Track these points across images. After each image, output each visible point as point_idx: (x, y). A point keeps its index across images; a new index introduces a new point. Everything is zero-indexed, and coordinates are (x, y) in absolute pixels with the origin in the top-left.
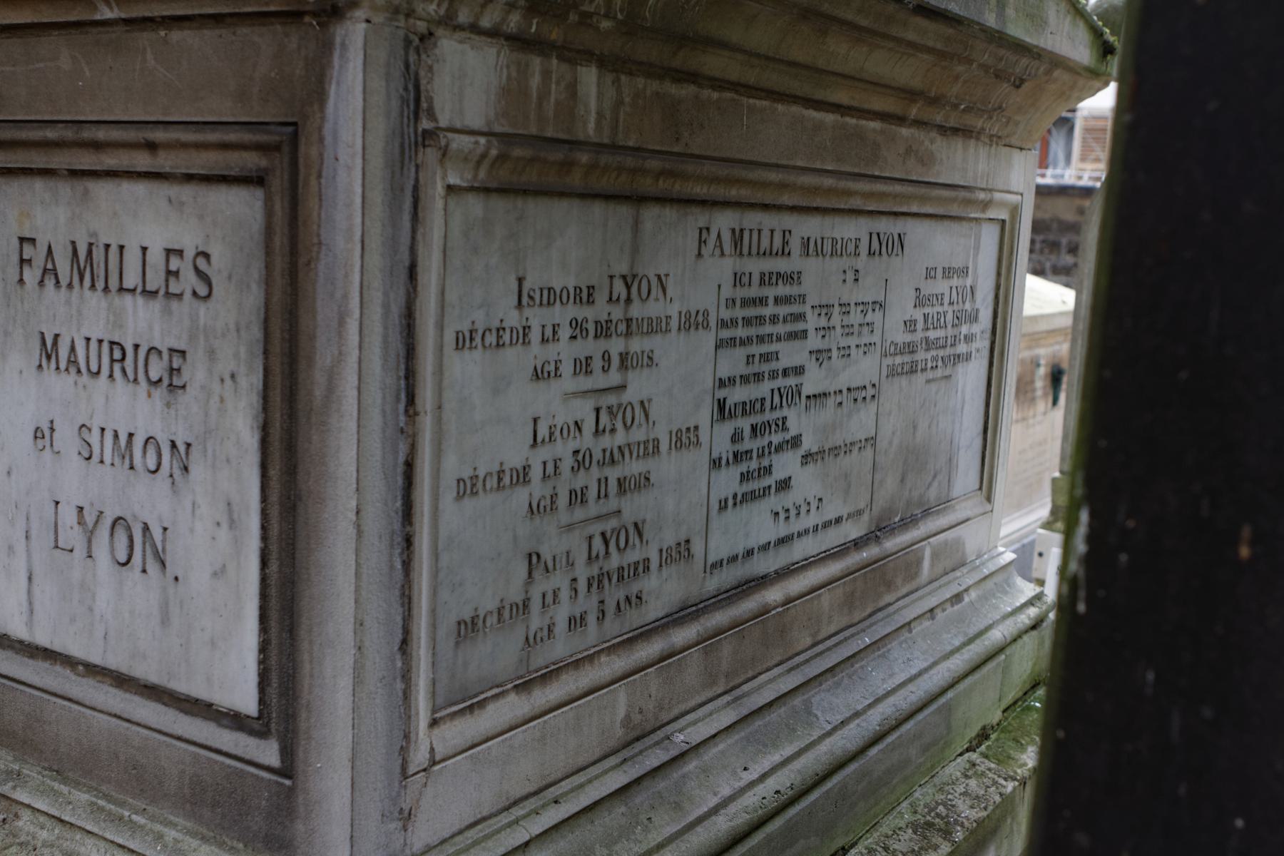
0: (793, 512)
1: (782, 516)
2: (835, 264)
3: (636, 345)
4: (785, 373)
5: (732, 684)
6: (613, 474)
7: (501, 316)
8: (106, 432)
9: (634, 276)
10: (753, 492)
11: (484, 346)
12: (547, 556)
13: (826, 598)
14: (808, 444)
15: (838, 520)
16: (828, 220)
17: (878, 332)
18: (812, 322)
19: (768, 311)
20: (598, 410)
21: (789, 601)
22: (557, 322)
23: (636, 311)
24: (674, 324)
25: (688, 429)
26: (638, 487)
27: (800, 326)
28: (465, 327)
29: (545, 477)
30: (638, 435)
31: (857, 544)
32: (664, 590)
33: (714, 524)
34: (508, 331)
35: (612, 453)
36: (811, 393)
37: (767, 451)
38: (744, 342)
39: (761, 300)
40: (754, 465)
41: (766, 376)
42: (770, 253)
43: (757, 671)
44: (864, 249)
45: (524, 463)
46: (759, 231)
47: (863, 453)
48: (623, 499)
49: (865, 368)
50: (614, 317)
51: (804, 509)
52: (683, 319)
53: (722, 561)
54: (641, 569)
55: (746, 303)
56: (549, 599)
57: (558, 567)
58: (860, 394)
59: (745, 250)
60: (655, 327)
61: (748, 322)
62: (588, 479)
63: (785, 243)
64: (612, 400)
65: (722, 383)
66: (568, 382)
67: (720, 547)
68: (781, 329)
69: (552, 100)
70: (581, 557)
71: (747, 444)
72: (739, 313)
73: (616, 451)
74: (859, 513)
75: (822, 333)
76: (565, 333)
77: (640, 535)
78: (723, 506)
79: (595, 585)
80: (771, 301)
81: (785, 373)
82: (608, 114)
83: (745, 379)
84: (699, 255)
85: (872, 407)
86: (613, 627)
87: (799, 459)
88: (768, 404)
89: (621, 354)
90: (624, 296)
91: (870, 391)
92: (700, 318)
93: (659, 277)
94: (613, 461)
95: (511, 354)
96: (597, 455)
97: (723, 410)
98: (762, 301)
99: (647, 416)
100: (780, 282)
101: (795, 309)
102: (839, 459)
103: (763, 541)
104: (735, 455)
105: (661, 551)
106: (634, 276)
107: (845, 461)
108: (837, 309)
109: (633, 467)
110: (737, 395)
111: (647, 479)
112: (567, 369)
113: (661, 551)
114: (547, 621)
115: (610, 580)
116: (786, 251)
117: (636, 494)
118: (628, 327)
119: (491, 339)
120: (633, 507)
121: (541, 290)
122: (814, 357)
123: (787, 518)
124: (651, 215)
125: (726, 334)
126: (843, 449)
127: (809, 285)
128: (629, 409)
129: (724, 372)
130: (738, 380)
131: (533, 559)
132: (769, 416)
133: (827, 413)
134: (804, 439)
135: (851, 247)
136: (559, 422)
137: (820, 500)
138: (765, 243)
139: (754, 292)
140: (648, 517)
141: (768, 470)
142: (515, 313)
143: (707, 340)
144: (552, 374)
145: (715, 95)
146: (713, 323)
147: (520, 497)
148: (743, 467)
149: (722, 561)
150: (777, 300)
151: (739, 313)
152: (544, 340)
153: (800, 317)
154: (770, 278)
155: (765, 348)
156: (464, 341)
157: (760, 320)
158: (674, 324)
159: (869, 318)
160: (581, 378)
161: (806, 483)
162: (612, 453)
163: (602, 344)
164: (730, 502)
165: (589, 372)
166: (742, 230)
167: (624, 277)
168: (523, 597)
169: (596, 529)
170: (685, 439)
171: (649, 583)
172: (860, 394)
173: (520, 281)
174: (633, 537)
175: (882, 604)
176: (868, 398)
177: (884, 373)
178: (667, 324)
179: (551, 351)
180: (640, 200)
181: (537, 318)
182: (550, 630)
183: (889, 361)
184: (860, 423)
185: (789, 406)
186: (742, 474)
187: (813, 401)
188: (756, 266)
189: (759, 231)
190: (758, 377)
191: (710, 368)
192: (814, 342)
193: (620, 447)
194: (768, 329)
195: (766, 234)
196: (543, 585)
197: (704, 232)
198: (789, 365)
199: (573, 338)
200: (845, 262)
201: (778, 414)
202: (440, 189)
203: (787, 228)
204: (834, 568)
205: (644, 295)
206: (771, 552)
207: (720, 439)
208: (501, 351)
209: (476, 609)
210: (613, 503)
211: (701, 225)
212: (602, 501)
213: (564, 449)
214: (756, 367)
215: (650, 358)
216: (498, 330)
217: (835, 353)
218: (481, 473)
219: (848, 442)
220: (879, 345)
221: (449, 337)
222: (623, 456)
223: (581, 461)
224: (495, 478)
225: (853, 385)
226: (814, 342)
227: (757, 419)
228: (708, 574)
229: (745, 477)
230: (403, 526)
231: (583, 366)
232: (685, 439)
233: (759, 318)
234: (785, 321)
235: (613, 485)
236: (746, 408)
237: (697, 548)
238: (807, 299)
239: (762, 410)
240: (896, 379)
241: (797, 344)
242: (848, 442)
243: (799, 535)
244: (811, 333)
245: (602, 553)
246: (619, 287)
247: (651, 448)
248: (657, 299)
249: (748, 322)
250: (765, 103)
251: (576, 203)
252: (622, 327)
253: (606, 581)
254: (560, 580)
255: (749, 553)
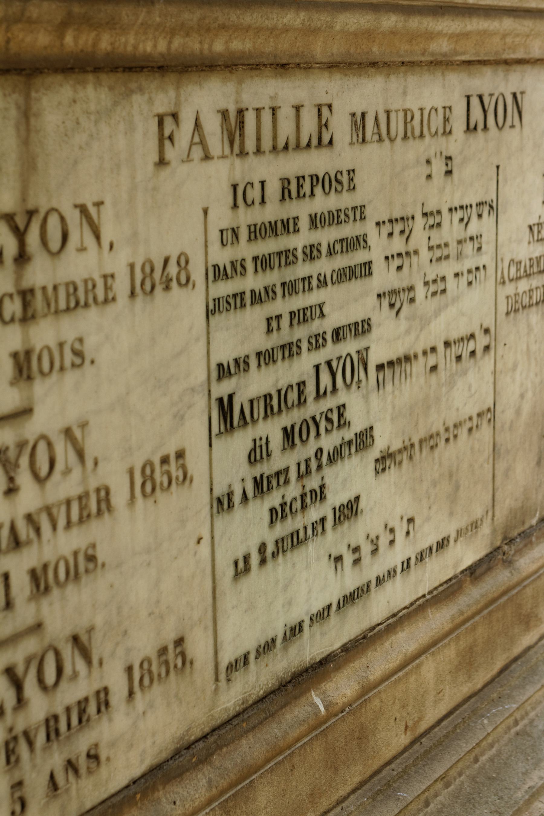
0: (366, 549)
1: (348, 559)
2: (414, 151)
4: (338, 335)
9: (31, 214)
13: (429, 668)
14: (383, 440)
15: (442, 544)
16: (395, 83)
17: (488, 248)
18: (378, 247)
19: (298, 242)
21: (367, 690)
24: (121, 287)
26: (74, 575)
27: (359, 257)
31: (475, 572)
35: (54, 527)
36: (384, 359)
37: (314, 465)
38: (257, 298)
39: (285, 224)
40: (293, 491)
41: (305, 346)
42: (298, 146)
44: (458, 124)
46: (274, 110)
47: (476, 434)
48: (45, 602)
49: (470, 307)
51: (383, 542)
52: (139, 276)
53: (246, 657)
54: (92, 708)
55: (256, 233)
58: (465, 348)
59: (250, 145)
60: (79, 298)
61: (263, 263)
63: (323, 126)
65: (223, 372)
67: (240, 633)
68: (325, 266)
71: (278, 461)
72: (246, 250)
74: (475, 525)
75: (397, 262)
77: (86, 655)
78: (242, 568)
80: (304, 223)
81: (338, 335)
83: (266, 357)
85: (487, 363)
87: (372, 465)
88: (310, 389)
89: (15, 355)
91: (482, 340)
92: (173, 269)
93: (83, 210)
97: (228, 415)
98: (288, 226)
100: (318, 190)
101: (348, 230)
102: (437, 452)
103: (317, 606)
104: (258, 483)
106: (31, 214)
107: (447, 453)
108: (420, 221)
109: (59, 545)
110: (257, 383)
111: (91, 558)
113: (129, 669)
115: (31, 743)
116: (326, 139)
118: (26, 305)
122: (385, 302)
123: (357, 562)
124: (57, 103)
126: (444, 436)
127: (367, 190)
128: (42, 447)
129: (225, 353)
132: (313, 408)
133: (412, 386)
134: (376, 433)
135: (437, 122)
137: (411, 520)
138: (286, 129)
139: (272, 212)
140: (99, 621)
141: (319, 494)
143: (191, 303)
146: (197, 274)
148: (274, 499)
149: (246, 657)
150: (315, 222)
151: (246, 250)
153: (358, 242)
154: (300, 186)
155: (299, 302)
157: (287, 257)
158: (121, 287)
159: (474, 228)
161: (384, 498)
162: (54, 527)
164: (255, 560)
170: (159, 476)
171: (105, 731)
172: (465, 348)
174: (72, 660)
175: (517, 650)
176: (479, 353)
177: (503, 308)
178: (107, 288)
183: (510, 289)
184: (468, 391)
185: (348, 386)
186: (272, 511)
187: (388, 372)
188: (271, 170)
189: (274, 110)
190: (290, 350)
191: (200, 348)
192: (384, 278)
194: (303, 269)
195: (286, 115)
197: (169, 123)
198: (344, 321)
200: (429, 146)
201: (330, 402)
203: (324, 100)
204: (439, 619)
205: (55, 243)
206: (334, 619)
211: (161, 110)
214: (286, 334)
215: (78, 353)
217: (420, 292)
219: (451, 424)
220: (491, 270)
222: (38, 530)
225: (454, 335)
226: (384, 278)
227: (293, 417)
228: (223, 683)
229: (276, 515)
232: (159, 476)
233: (285, 255)
234: (331, 252)
236: (271, 404)
237: (199, 648)
238: (368, 212)
239: (301, 402)
240: (521, 315)
241: (355, 286)
242: (451, 424)
243: (380, 581)
244: (379, 266)
245: (330, 388)
247: (99, 504)
248: (82, 249)
249: (263, 263)
253: (23, 748)
255: (295, 631)
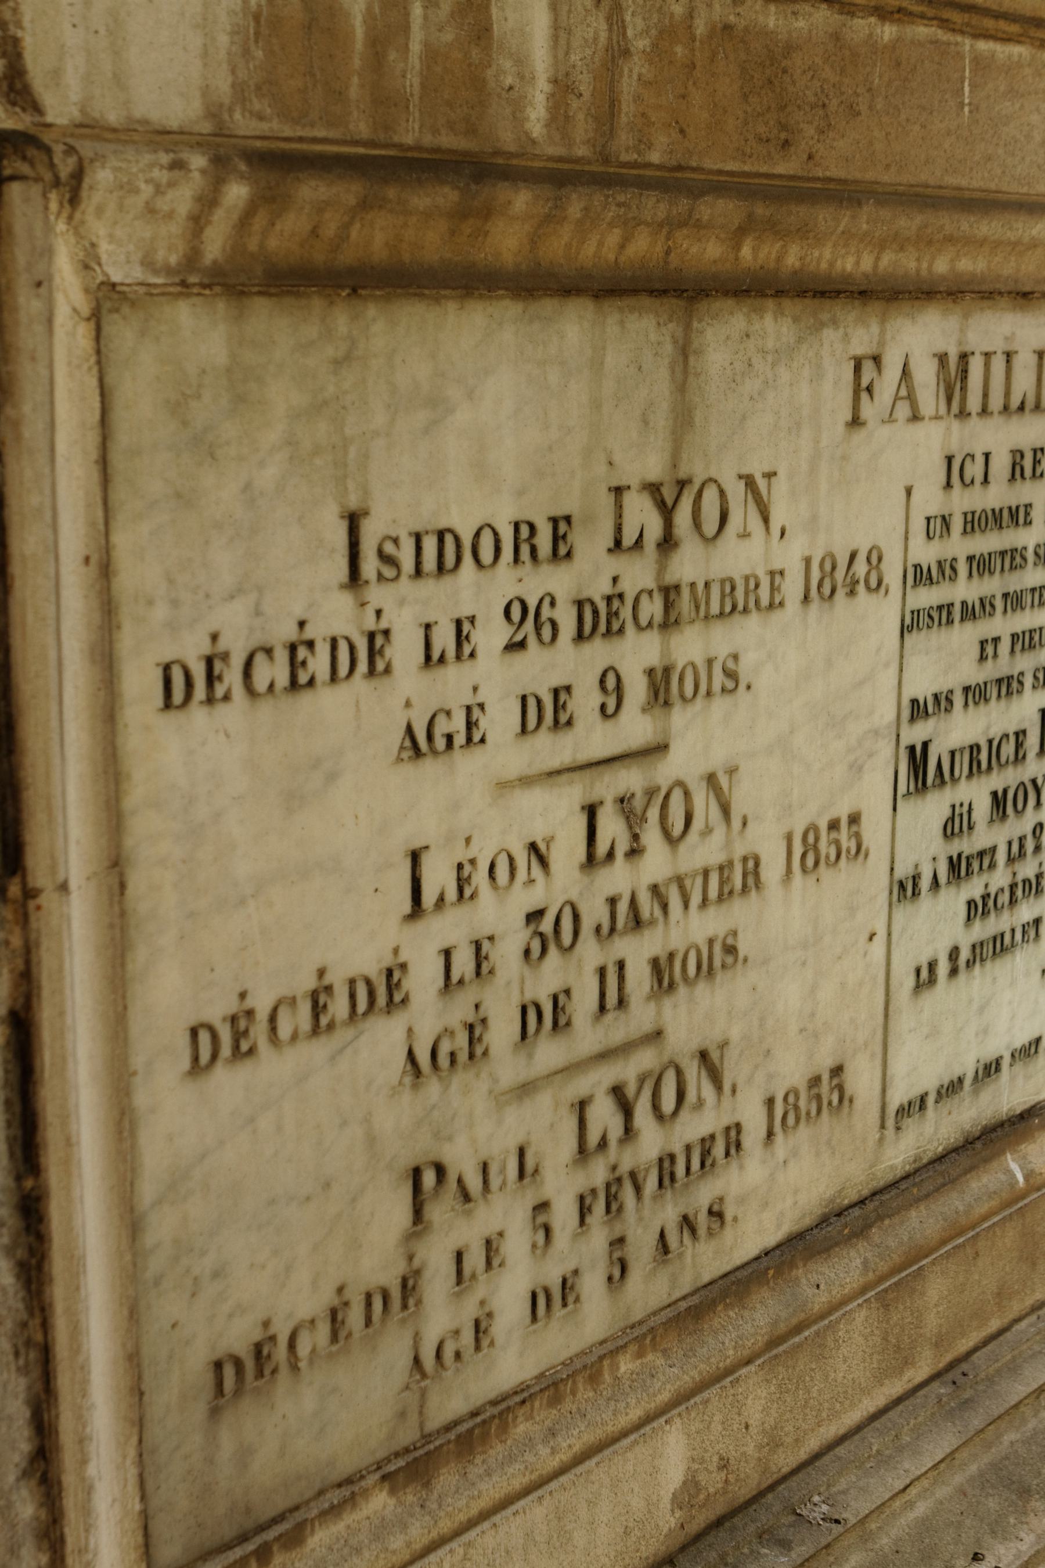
3: (690, 646)
5: (949, 1357)
6: (637, 952)
7: (298, 611)
8: (1018, 362)
9: (682, 484)
10: (998, 939)
11: (250, 691)
12: (462, 1161)
20: (591, 811)
22: (465, 611)
23: (689, 565)
24: (792, 588)
25: (834, 825)
26: (707, 970)
28: (192, 650)
29: (449, 984)
30: (703, 851)
32: (774, 1191)
33: (905, 1021)
34: (323, 651)
40: (1000, 879)
43: (1011, 1316)
45: (388, 961)
46: (1009, 356)
48: (667, 1003)
50: (629, 587)
55: (973, 523)
56: (475, 1260)
57: (495, 1182)
59: (974, 403)
60: (737, 600)
61: (980, 565)
62: (576, 973)
64: (630, 779)
65: (918, 710)
66: (505, 751)
67: (917, 1069)
69: (416, 47)
70: (556, 1150)
71: (984, 835)
72: (959, 546)
73: (645, 900)
76: (489, 636)
77: (716, 1077)
78: (925, 979)
79: (600, 1207)
82: (585, 84)
84: (856, 422)
86: (649, 1291)
89: (650, 672)
90: (654, 530)
92: (861, 568)
93: (749, 481)
94: (637, 922)
95: (332, 704)
96: (594, 912)
97: (920, 769)
99: (726, 810)
105: (770, 1102)
109: (692, 928)
111: (731, 950)
112: (500, 720)
113: (770, 1102)
114: (470, 1310)
115: (638, 1189)
117: (701, 987)
118: (668, 606)
119: (273, 672)
120: (689, 1020)
121: (418, 538)
124: (727, 337)
125: (926, 598)
128: (677, 796)
129: (922, 683)
130: (958, 699)
131: (426, 1183)
136: (484, 852)
140: (735, 1034)
142: (345, 601)
143: (882, 614)
144: (460, 739)
145: (888, 32)
146: (893, 576)
147: (384, 1040)
148: (974, 889)
149: (923, 1099)
151: (959, 546)
152: (430, 660)
156: (177, 689)
158: (792, 588)
160: (543, 739)
163: (599, 653)
165: (562, 723)
166: (964, 357)
167: (653, 489)
168: (400, 1268)
169: (597, 1081)
170: (826, 845)
171: (738, 1181)
173: (354, 521)
178: (773, 589)
179: (453, 685)
180: (681, 292)
181: (406, 608)
182: (479, 1328)
186: (971, 904)
189: (1009, 356)
190: (1008, 686)
193: (655, 889)
196: (453, 1230)
197: (868, 367)
199: (516, 646)
202: (69, 291)
205: (710, 527)
207: (918, 833)
208: (306, 698)
209: (266, 1324)
210: (641, 1015)
211: (859, 351)
212: (609, 1017)
213: (499, 914)
214: (1003, 665)
215: (730, 674)
216: (293, 648)
218: (262, 1005)
221: (140, 682)
222: (665, 907)
223: (548, 933)
224: (305, 1009)
229: (975, 910)
230: (19, 1178)
231: (547, 711)
232: (826, 845)
235: (639, 977)
236: (977, 759)
237: (862, 1081)
239: (1019, 758)
245: (616, 1130)
246: (642, 515)
247: (741, 878)
248: (745, 535)
249: (980, 565)
250: (1018, 51)
251: (509, 309)
252: (652, 608)
253: (628, 1193)
254: (506, 1214)
255: (991, 1069)
